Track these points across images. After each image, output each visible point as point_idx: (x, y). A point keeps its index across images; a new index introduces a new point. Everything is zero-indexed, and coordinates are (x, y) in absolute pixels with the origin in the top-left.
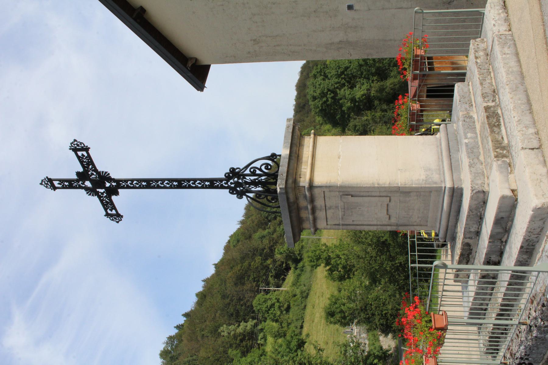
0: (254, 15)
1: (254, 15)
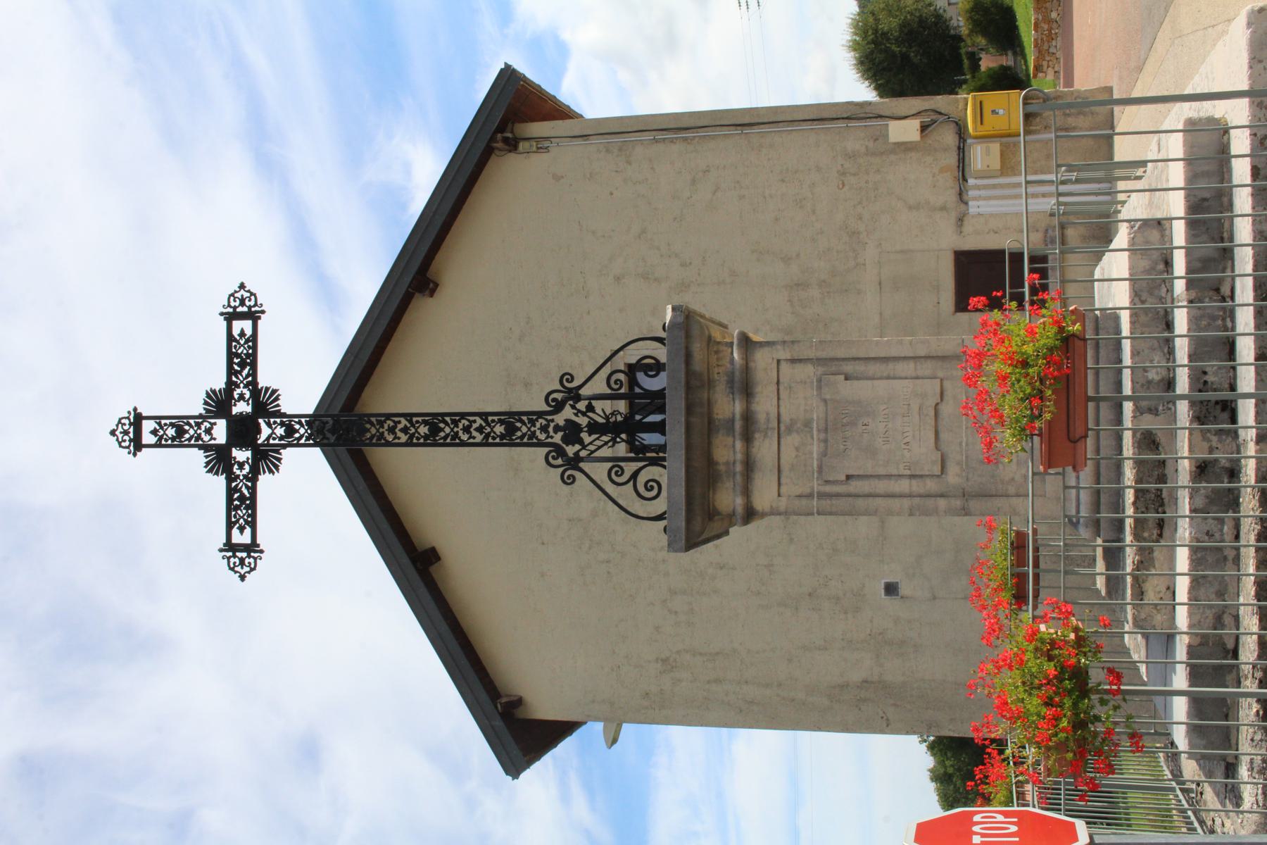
0: (673, 592)
1: (673, 592)
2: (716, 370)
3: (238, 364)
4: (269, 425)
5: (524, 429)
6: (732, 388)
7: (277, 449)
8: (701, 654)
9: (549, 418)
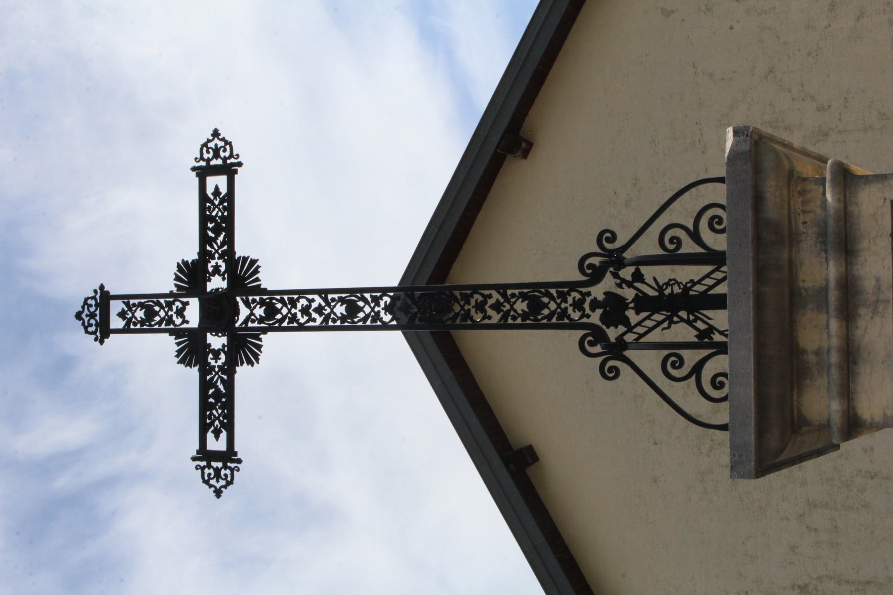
2: (801, 219)
3: (212, 230)
4: (247, 304)
5: (553, 306)
6: (824, 243)
7: (257, 333)
8: (847, 582)
9: (584, 290)
